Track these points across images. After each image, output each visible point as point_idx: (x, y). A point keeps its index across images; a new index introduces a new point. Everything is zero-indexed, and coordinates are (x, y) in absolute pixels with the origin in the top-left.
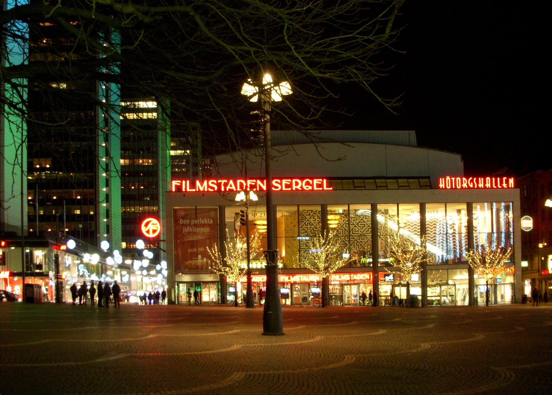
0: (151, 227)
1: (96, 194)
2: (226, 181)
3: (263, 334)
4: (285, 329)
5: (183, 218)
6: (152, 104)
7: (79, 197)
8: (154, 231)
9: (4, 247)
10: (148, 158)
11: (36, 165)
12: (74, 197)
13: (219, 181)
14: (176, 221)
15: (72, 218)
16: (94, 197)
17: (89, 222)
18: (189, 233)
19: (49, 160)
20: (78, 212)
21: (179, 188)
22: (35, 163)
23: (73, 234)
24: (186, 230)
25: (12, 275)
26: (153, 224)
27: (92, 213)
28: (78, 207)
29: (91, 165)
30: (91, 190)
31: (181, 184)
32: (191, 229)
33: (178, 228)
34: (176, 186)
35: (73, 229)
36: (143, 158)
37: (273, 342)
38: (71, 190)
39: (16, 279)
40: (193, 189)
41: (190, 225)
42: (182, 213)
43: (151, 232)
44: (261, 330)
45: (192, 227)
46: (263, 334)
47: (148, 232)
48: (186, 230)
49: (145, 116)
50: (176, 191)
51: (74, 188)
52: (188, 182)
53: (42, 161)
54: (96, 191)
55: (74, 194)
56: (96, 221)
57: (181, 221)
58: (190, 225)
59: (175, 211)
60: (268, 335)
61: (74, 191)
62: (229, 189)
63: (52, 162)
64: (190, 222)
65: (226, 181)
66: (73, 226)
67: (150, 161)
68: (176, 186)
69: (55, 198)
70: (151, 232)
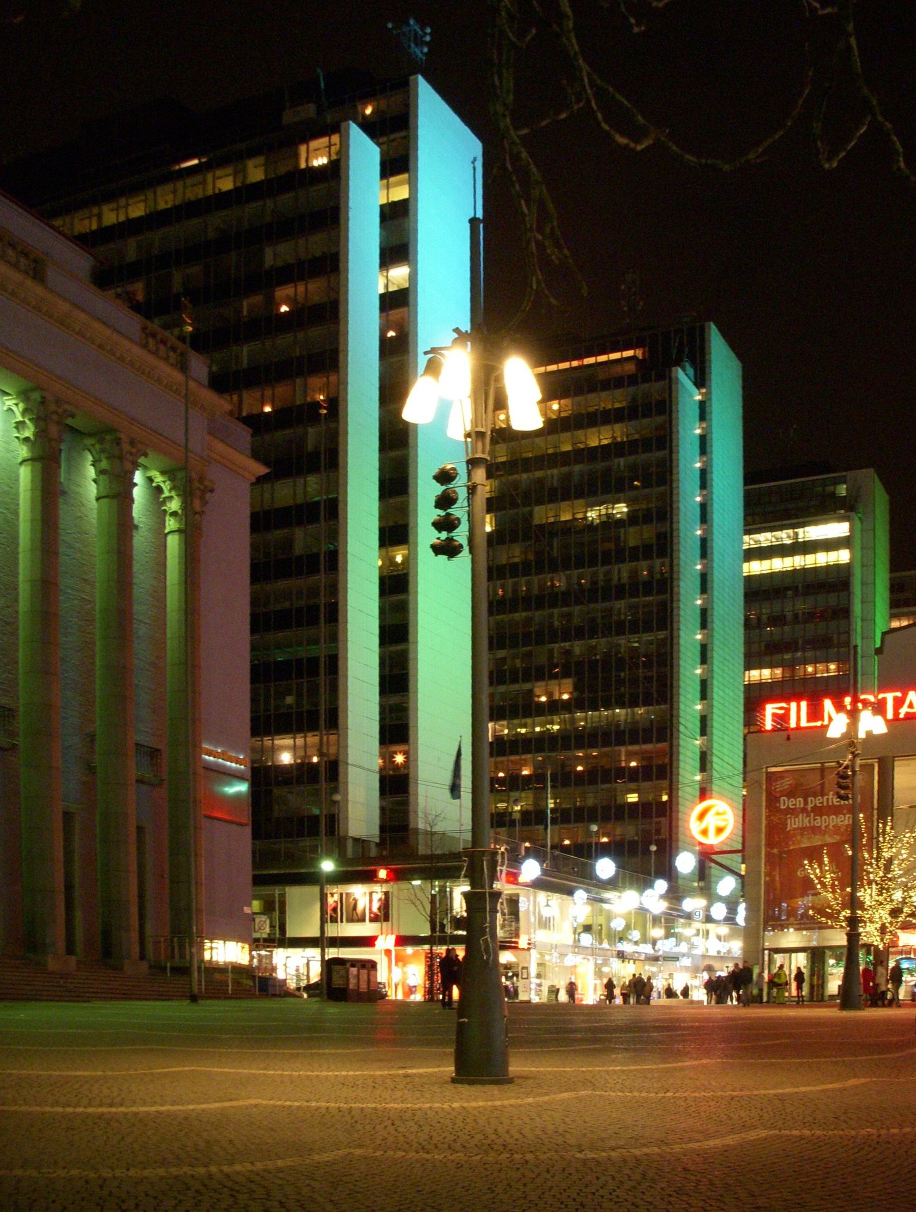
0: (711, 821)
1: (671, 755)
2: (899, 694)
3: (453, 1081)
4: (515, 1067)
5: (791, 794)
6: (838, 529)
7: (633, 764)
8: (720, 830)
9: (385, 881)
10: (828, 661)
11: (539, 696)
12: (623, 764)
13: (881, 696)
14: (772, 800)
15: (616, 812)
16: (667, 760)
17: (655, 820)
18: (802, 829)
19: (568, 683)
20: (633, 798)
21: (782, 719)
22: (537, 691)
23: (614, 850)
24: (793, 823)
25: (402, 941)
26: (718, 814)
27: (665, 798)
28: (633, 785)
29: (660, 686)
30: (660, 745)
31: (788, 710)
32: (806, 820)
33: (775, 819)
34: (774, 715)
35: (618, 838)
36: (815, 662)
37: (477, 1101)
38: (616, 748)
39: (409, 950)
40: (816, 720)
41: (804, 810)
42: (787, 782)
43: (712, 832)
44: (450, 1069)
45: (808, 816)
46: (453, 1081)
47: (705, 832)
48: (793, 823)
49: (822, 559)
50: (774, 730)
51: (623, 743)
52: (804, 704)
53: (554, 686)
54: (671, 746)
55: (623, 758)
56: (671, 816)
57: (785, 803)
58: (804, 810)
59: (770, 777)
60: (471, 1083)
61: (623, 749)
62: (907, 714)
63: (576, 688)
64: (806, 803)
65: (899, 694)
66: (618, 831)
67: (832, 667)
68: (774, 715)
69: (580, 768)
70: (712, 832)
